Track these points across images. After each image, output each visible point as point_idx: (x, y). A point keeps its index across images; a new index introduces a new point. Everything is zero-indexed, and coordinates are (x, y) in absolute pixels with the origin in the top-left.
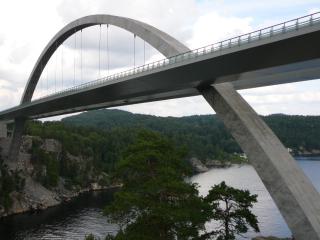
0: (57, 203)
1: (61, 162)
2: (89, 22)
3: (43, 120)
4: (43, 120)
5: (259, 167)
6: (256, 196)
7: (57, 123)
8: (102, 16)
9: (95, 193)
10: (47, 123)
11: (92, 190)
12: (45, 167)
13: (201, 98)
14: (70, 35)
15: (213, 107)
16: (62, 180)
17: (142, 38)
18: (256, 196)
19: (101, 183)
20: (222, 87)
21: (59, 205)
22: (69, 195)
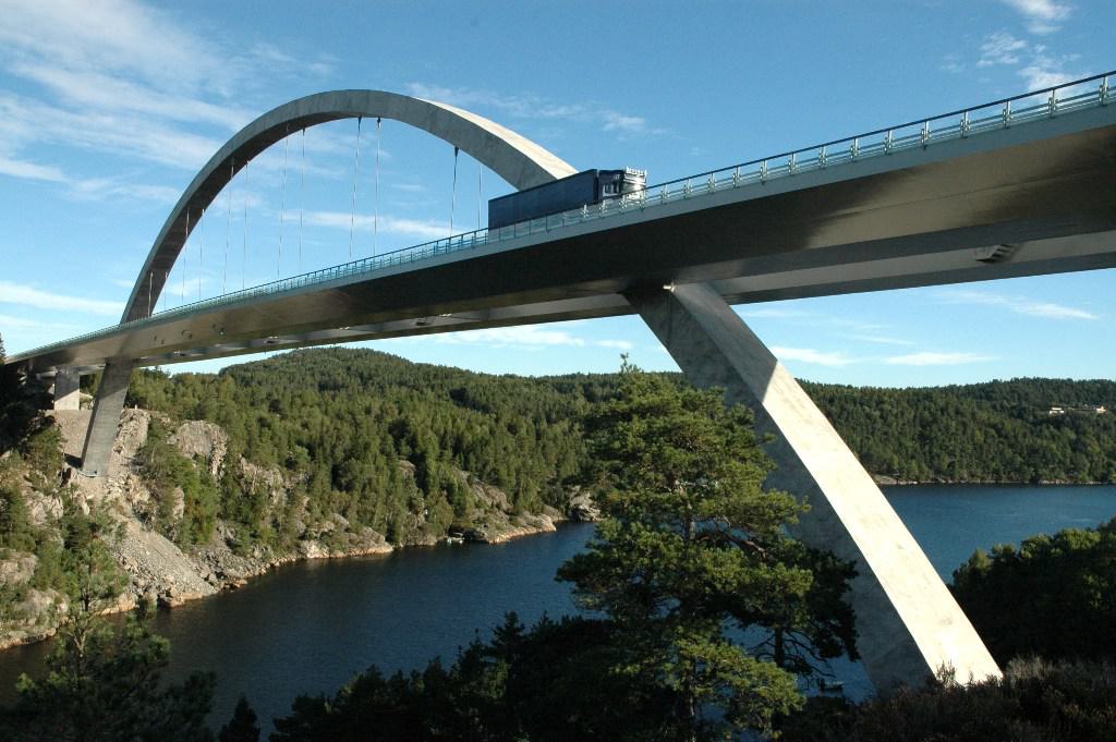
0: (213, 591)
1: (223, 482)
2: (303, 112)
3: (173, 369)
4: (173, 369)
5: (880, 402)
6: (859, 658)
7: (204, 379)
8: (366, 94)
9: (311, 565)
10: (180, 379)
11: (303, 561)
12: (179, 491)
13: (635, 322)
14: (867, 244)
15: (675, 357)
16: (223, 530)
17: (475, 155)
18: (859, 658)
19: (325, 538)
20: (683, 291)
21: (218, 595)
22: (241, 572)
